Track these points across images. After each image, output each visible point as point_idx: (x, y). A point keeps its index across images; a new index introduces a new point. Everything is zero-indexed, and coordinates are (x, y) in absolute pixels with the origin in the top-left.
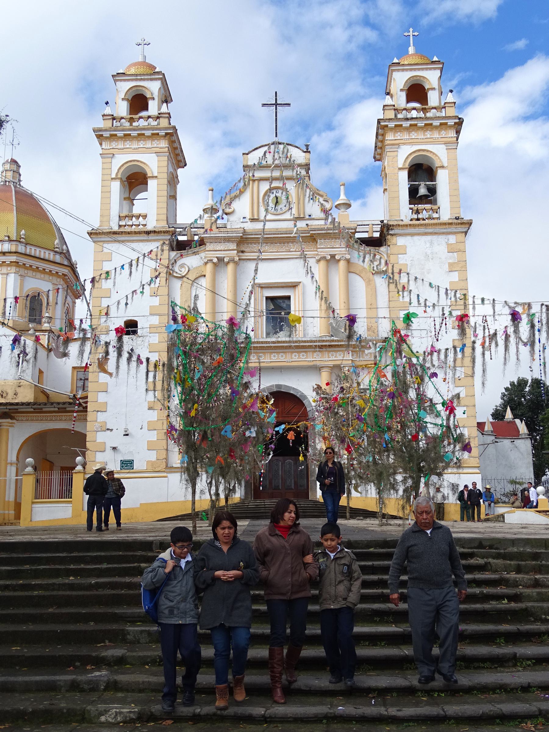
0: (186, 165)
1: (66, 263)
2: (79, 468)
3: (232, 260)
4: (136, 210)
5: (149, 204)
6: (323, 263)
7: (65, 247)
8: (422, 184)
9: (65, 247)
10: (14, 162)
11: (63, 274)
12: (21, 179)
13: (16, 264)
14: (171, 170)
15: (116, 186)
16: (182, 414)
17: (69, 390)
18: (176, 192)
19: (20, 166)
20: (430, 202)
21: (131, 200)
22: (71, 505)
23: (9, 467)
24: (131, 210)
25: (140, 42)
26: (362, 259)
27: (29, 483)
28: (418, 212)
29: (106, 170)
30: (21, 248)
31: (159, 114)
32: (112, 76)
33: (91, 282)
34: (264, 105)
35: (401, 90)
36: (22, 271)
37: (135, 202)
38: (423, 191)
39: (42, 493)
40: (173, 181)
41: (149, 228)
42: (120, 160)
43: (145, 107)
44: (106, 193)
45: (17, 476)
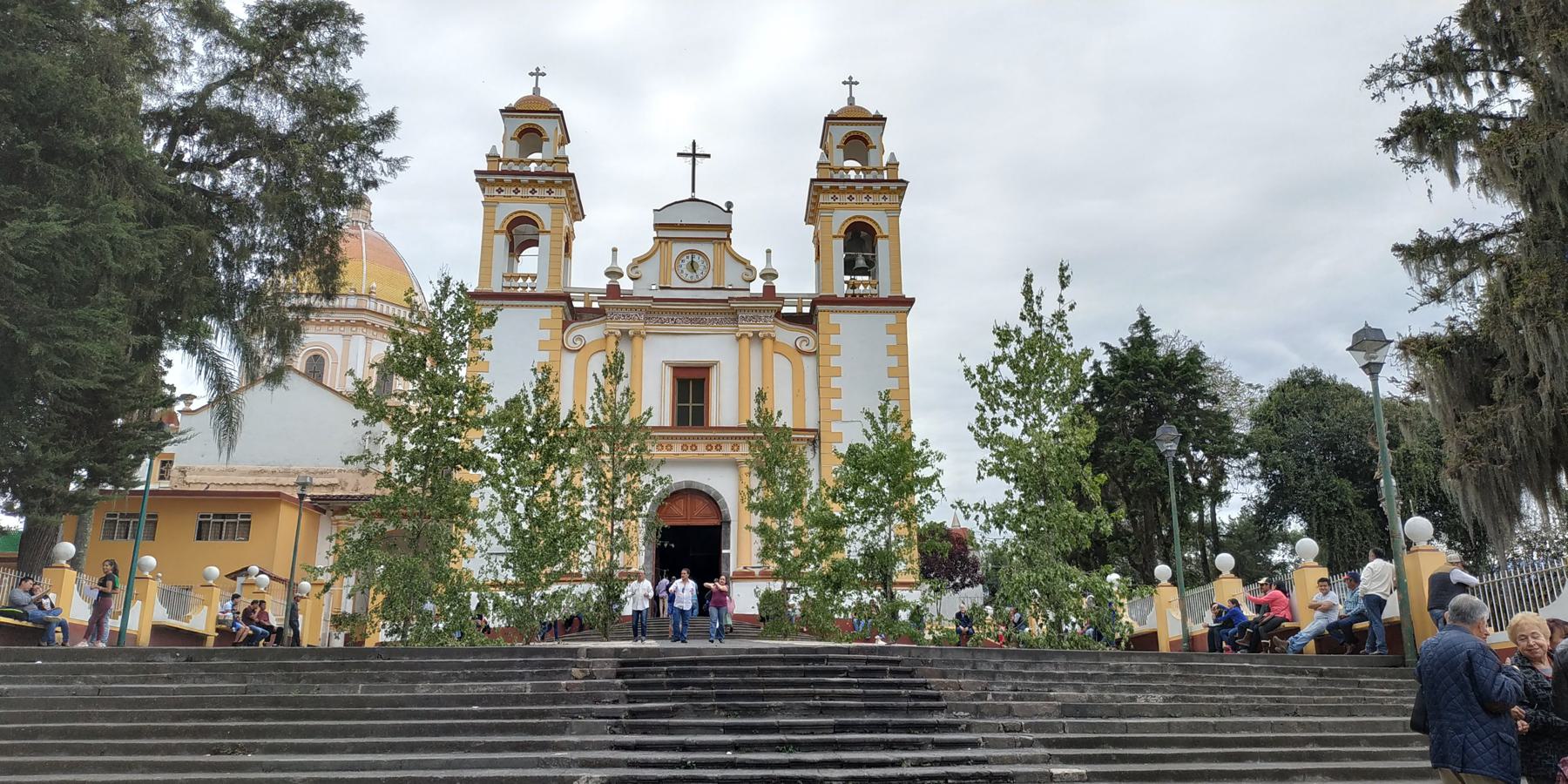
3: (638, 334)
6: (745, 341)
15: (501, 241)
20: (868, 274)
26: (788, 336)
30: (371, 305)
34: (680, 155)
36: (370, 333)
38: (861, 263)
41: (539, 291)
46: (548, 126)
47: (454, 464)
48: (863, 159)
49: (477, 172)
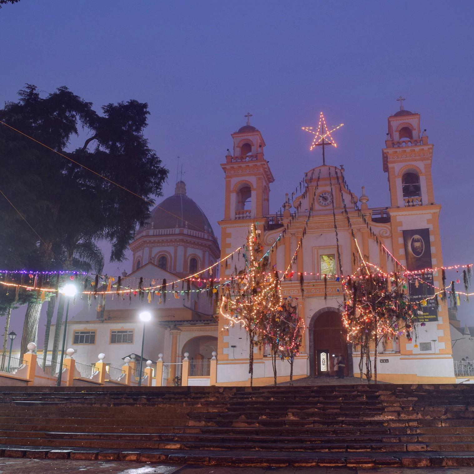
0: (274, 180)
1: (210, 238)
2: (214, 358)
4: (246, 208)
5: (252, 204)
7: (210, 230)
8: (411, 185)
9: (210, 230)
10: (182, 182)
11: (209, 245)
12: (186, 192)
13: (182, 240)
14: (264, 184)
15: (234, 197)
16: (412, 388)
17: (306, 374)
18: (268, 197)
19: (185, 185)
21: (243, 203)
22: (209, 379)
23: (177, 358)
24: (243, 208)
25: (247, 115)
27: (186, 364)
28: (408, 202)
29: (228, 184)
31: (257, 154)
32: (231, 134)
33: (133, 255)
35: (396, 131)
37: (245, 203)
38: (412, 189)
39: (192, 372)
40: (266, 190)
42: (235, 181)
43: (250, 150)
44: (228, 200)
45: (182, 364)
46: (253, 138)
47: (384, 423)
48: (410, 136)
49: (221, 165)
